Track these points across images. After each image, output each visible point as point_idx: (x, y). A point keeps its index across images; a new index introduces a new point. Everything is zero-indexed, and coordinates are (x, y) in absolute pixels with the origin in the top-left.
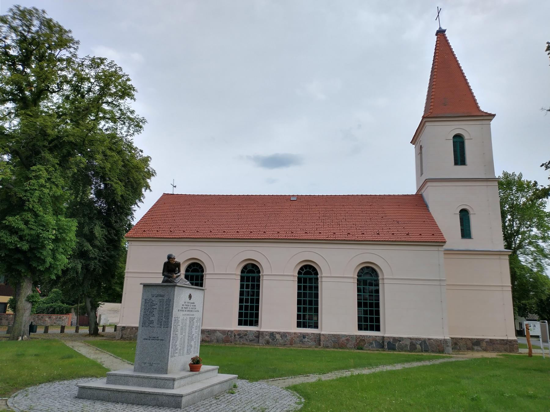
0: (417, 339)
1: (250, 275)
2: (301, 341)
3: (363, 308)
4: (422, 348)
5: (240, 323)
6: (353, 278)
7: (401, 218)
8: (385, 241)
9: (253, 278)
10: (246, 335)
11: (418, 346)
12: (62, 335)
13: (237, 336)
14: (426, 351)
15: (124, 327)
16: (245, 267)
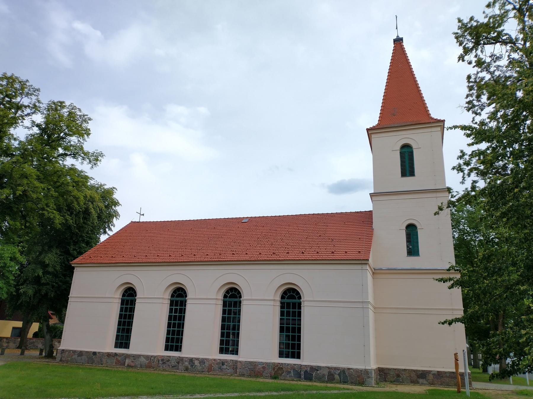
0: (336, 369)
1: (178, 299)
2: (220, 368)
3: (285, 334)
4: (340, 378)
5: (167, 349)
6: (71, 297)
7: (336, 238)
8: (307, 260)
9: (294, 304)
10: (169, 361)
11: (337, 377)
12: (22, 356)
13: (160, 362)
14: (345, 382)
15: (63, 350)
16: (227, 292)
